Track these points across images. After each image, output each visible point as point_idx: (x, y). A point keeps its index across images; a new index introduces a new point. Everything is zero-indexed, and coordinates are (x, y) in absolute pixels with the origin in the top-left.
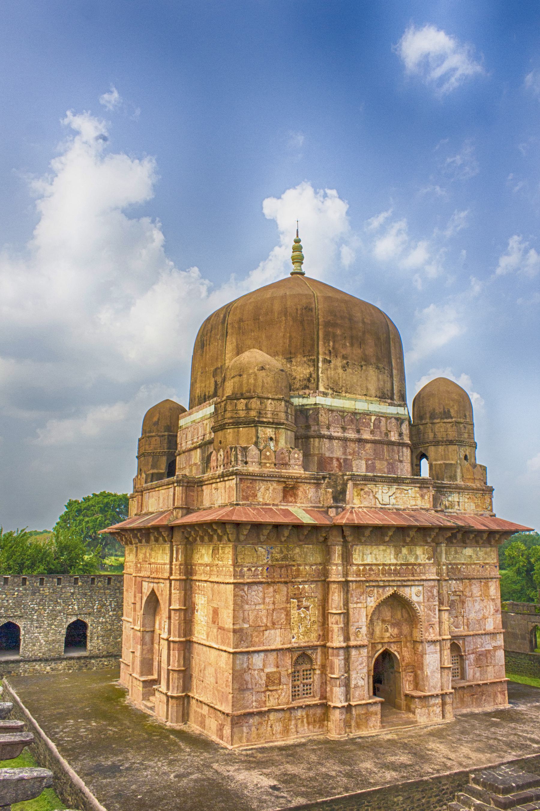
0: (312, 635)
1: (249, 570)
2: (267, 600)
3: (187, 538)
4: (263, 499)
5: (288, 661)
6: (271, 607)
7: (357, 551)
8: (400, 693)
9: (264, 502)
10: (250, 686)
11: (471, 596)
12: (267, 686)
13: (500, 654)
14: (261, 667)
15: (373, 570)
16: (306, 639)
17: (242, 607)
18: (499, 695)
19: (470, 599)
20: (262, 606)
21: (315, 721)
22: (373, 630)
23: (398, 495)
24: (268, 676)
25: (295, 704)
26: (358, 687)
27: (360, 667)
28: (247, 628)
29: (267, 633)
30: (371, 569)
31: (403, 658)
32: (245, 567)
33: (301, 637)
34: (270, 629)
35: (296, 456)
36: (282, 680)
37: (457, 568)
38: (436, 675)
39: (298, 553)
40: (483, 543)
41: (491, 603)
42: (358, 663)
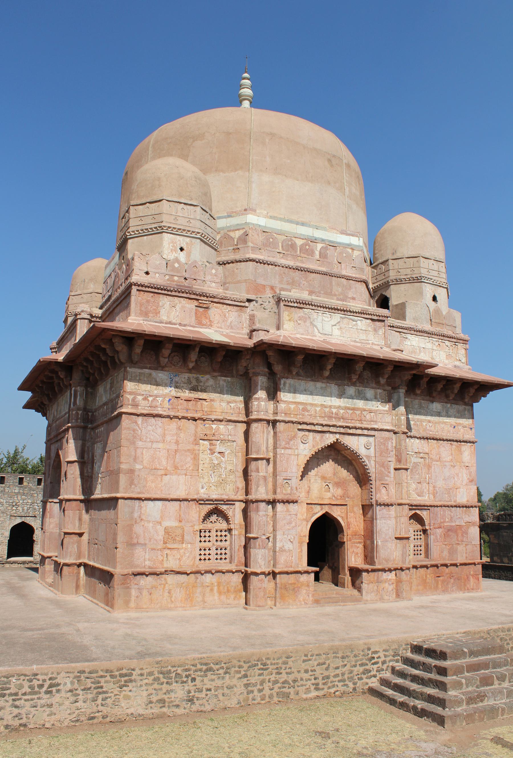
0: (228, 487)
1: (145, 399)
2: (168, 438)
3: (88, 379)
4: (168, 317)
5: (196, 513)
6: (174, 447)
7: (287, 385)
8: (344, 568)
9: (169, 321)
10: (141, 541)
11: (439, 460)
12: (165, 543)
13: (475, 532)
14: (158, 519)
15: (308, 411)
16: (220, 491)
17: (134, 443)
18: (471, 579)
19: (438, 463)
20: (160, 445)
21: (228, 591)
22: (309, 487)
23: (343, 326)
24: (167, 531)
25: (203, 566)
26: (285, 551)
27: (288, 527)
28: (140, 470)
29: (166, 478)
30: (304, 410)
31: (348, 524)
32: (140, 395)
33: (213, 487)
34: (171, 474)
35: (214, 271)
36: (186, 537)
37: (422, 425)
38: (389, 545)
39: (212, 386)
40: (454, 399)
41: (464, 471)
42: (285, 522)
